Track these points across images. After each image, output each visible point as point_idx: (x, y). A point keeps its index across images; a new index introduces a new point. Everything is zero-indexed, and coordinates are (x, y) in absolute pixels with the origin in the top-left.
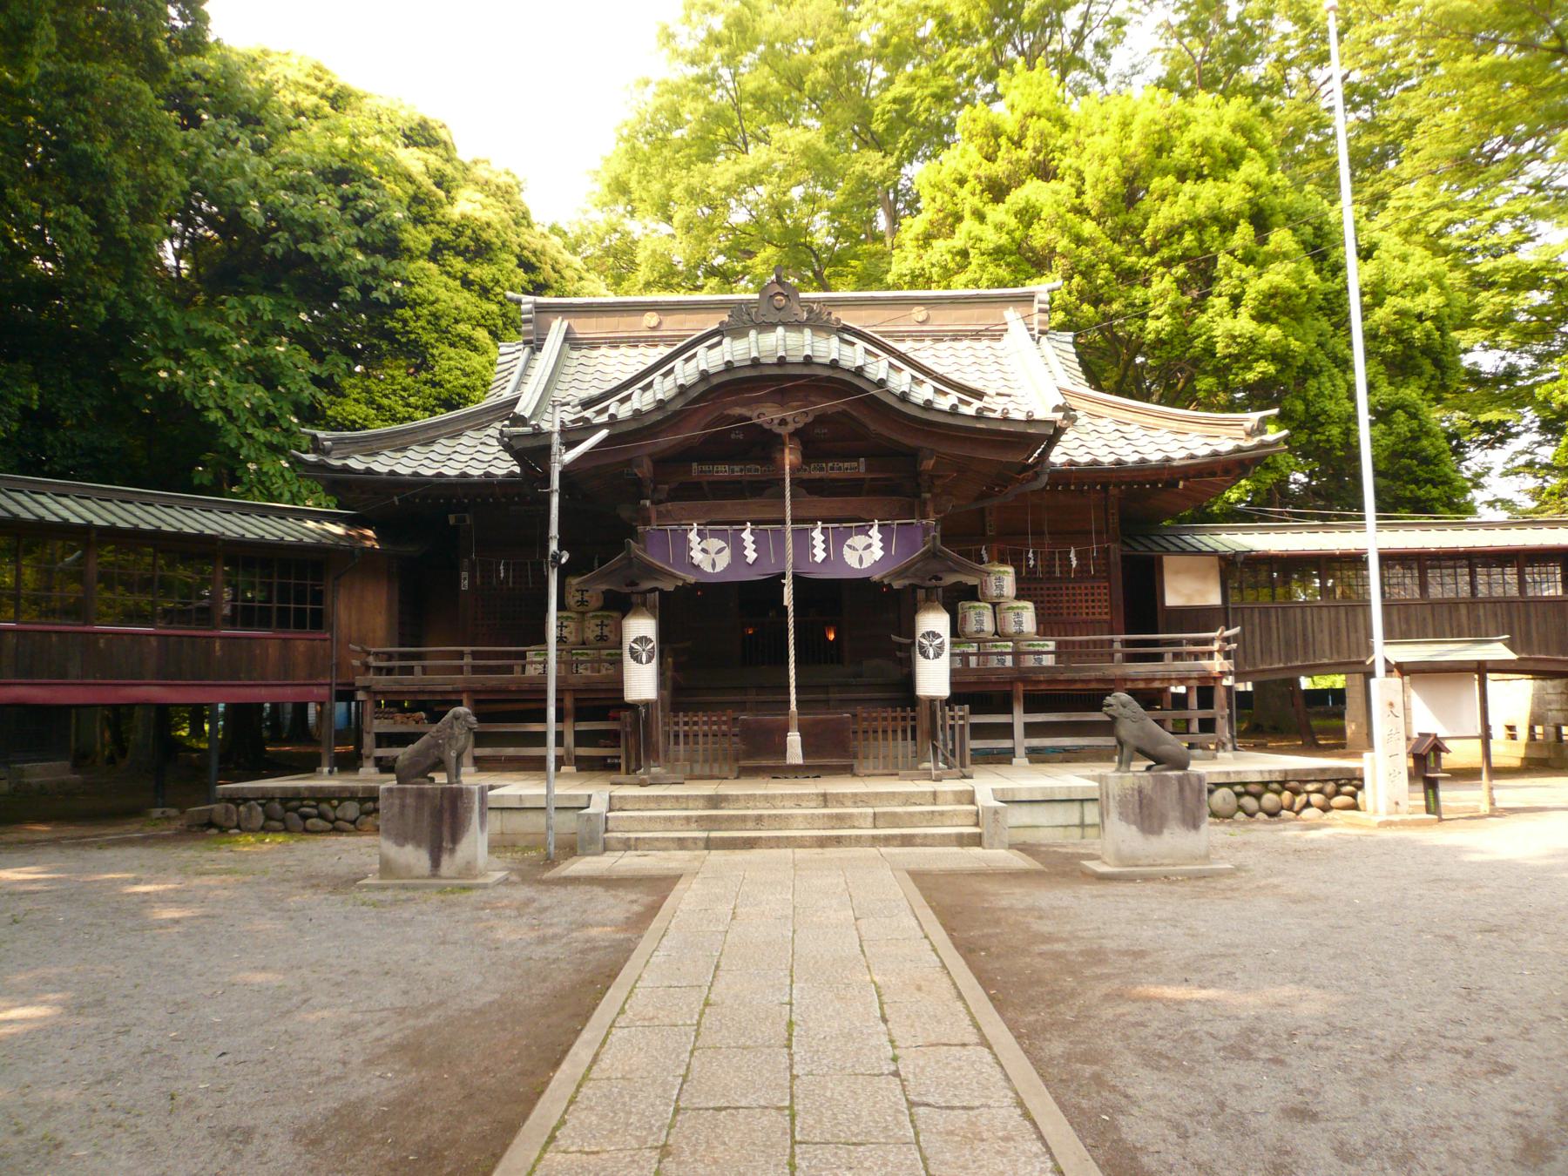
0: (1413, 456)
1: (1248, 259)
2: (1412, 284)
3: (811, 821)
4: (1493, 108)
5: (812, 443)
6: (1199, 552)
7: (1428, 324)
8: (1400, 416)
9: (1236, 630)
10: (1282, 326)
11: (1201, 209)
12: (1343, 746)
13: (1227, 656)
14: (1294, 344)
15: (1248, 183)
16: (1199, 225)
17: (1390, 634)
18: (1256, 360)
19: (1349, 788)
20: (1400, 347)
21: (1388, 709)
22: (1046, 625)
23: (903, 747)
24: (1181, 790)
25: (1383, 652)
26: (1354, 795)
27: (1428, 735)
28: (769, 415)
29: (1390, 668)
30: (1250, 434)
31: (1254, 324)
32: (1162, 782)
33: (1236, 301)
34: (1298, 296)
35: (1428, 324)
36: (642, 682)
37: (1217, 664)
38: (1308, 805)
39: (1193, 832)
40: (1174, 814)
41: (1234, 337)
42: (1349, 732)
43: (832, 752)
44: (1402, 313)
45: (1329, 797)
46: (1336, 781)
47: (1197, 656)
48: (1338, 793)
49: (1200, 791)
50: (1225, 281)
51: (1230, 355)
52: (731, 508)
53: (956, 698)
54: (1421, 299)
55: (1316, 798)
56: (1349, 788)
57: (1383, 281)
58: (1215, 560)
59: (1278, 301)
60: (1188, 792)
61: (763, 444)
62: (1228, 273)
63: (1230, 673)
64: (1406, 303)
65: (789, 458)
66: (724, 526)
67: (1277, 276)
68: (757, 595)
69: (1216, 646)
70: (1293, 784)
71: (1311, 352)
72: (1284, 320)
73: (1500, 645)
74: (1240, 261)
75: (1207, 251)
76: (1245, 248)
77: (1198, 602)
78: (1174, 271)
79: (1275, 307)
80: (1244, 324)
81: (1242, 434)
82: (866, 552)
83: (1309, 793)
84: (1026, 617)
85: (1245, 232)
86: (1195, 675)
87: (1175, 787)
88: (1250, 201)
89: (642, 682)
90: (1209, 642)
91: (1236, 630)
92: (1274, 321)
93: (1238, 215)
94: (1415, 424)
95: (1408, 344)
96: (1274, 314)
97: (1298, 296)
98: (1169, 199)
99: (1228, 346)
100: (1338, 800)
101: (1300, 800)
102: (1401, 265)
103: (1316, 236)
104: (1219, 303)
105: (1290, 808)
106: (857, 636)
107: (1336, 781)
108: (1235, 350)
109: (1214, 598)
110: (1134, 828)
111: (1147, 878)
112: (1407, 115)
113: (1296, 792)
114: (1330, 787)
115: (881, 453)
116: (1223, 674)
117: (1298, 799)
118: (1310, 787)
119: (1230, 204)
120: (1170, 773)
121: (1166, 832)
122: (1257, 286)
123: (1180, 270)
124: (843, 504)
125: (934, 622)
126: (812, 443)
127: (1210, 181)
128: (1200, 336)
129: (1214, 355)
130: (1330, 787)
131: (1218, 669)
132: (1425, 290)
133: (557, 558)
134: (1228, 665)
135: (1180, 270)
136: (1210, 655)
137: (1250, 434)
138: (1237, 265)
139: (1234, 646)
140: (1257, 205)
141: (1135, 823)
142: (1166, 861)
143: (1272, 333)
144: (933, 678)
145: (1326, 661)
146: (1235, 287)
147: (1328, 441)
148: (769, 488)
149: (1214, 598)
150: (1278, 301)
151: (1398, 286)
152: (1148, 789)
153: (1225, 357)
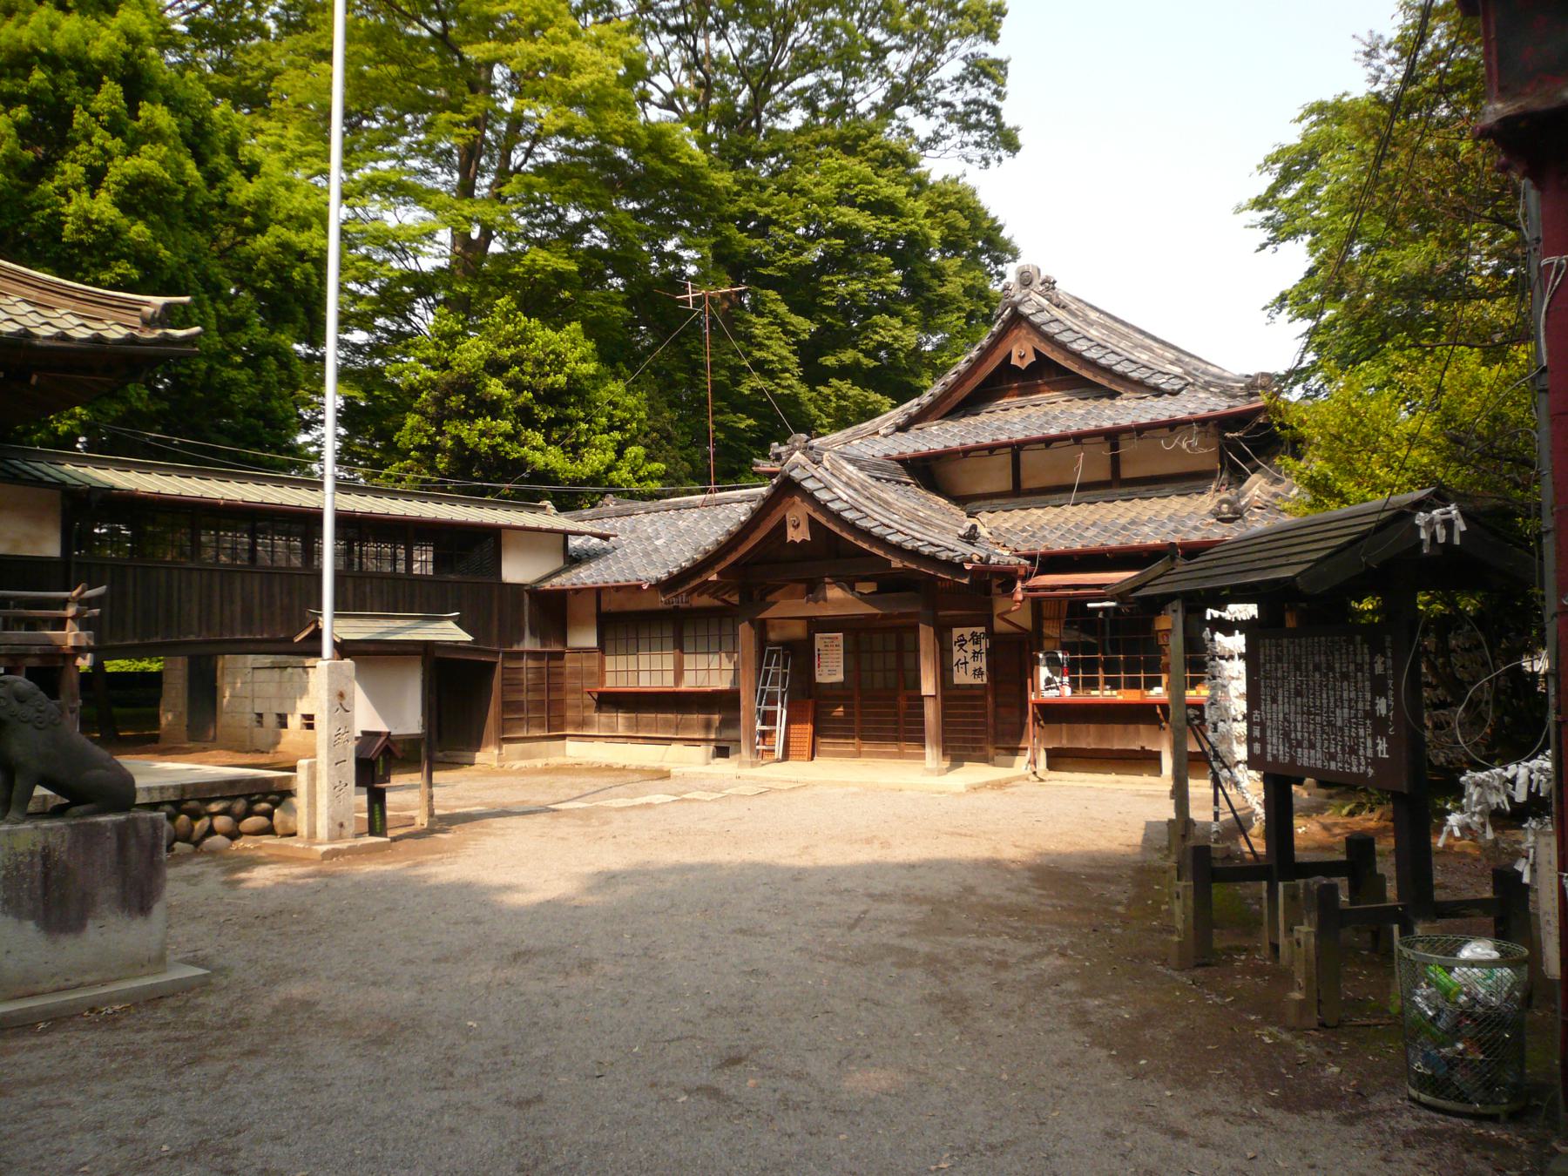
0: (261, 415)
1: (115, 128)
2: (297, 217)
6: (39, 482)
7: (308, 265)
8: (271, 363)
9: (101, 590)
10: (150, 225)
11: (60, 42)
12: (155, 739)
13: (85, 624)
14: (164, 253)
15: (126, 33)
16: (53, 61)
17: (343, 607)
18: (117, 259)
19: (264, 806)
20: (279, 285)
21: (337, 701)
24: (122, 848)
25: (332, 627)
26: (269, 815)
27: (378, 734)
29: (344, 649)
30: (149, 323)
31: (116, 211)
32: (90, 836)
33: (95, 178)
34: (174, 192)
35: (308, 265)
37: (71, 636)
38: (211, 831)
39: (140, 919)
40: (107, 892)
41: (88, 221)
42: (163, 721)
44: (285, 247)
45: (239, 819)
46: (248, 797)
47: (32, 624)
48: (249, 813)
49: (155, 847)
50: (83, 147)
51: (80, 244)
54: (305, 236)
55: (221, 822)
56: (264, 806)
57: (268, 203)
58: (58, 493)
59: (148, 191)
60: (133, 851)
62: (88, 137)
63: (90, 649)
64: (291, 236)
67: (147, 161)
69: (71, 611)
70: (192, 804)
71: (181, 268)
72: (154, 218)
73: (450, 624)
74: (104, 128)
75: (61, 99)
76: (112, 114)
77: (27, 551)
78: (12, 112)
79: (144, 198)
80: (103, 207)
81: (137, 321)
83: (213, 815)
85: (109, 95)
86: (36, 650)
87: (112, 844)
88: (126, 55)
90: (64, 603)
91: (101, 590)
92: (142, 217)
93: (106, 66)
94: (284, 375)
95: (287, 282)
96: (142, 208)
97: (174, 192)
98: (19, 16)
99: (79, 231)
100: (251, 822)
101: (201, 825)
102: (287, 194)
103: (195, 134)
104: (71, 170)
105: (186, 838)
107: (248, 797)
108: (88, 238)
109: (51, 548)
110: (30, 925)
111: (57, 1020)
112: (267, 64)
113: (195, 816)
114: (240, 806)
116: (78, 651)
117: (198, 825)
118: (214, 807)
119: (98, 51)
120: (102, 819)
121: (91, 926)
122: (124, 168)
123: (22, 113)
127: (75, 17)
128: (42, 208)
129: (58, 239)
130: (240, 806)
131: (71, 642)
132: (310, 228)
134: (85, 638)
135: (22, 113)
136: (60, 624)
137: (149, 323)
138: (100, 131)
139: (96, 611)
140: (134, 65)
141: (32, 916)
142: (88, 978)
143: (138, 231)
145: (192, 638)
146: (95, 157)
147: (191, 376)
149: (51, 548)
150: (148, 191)
151: (281, 216)
152: (61, 849)
153: (73, 245)
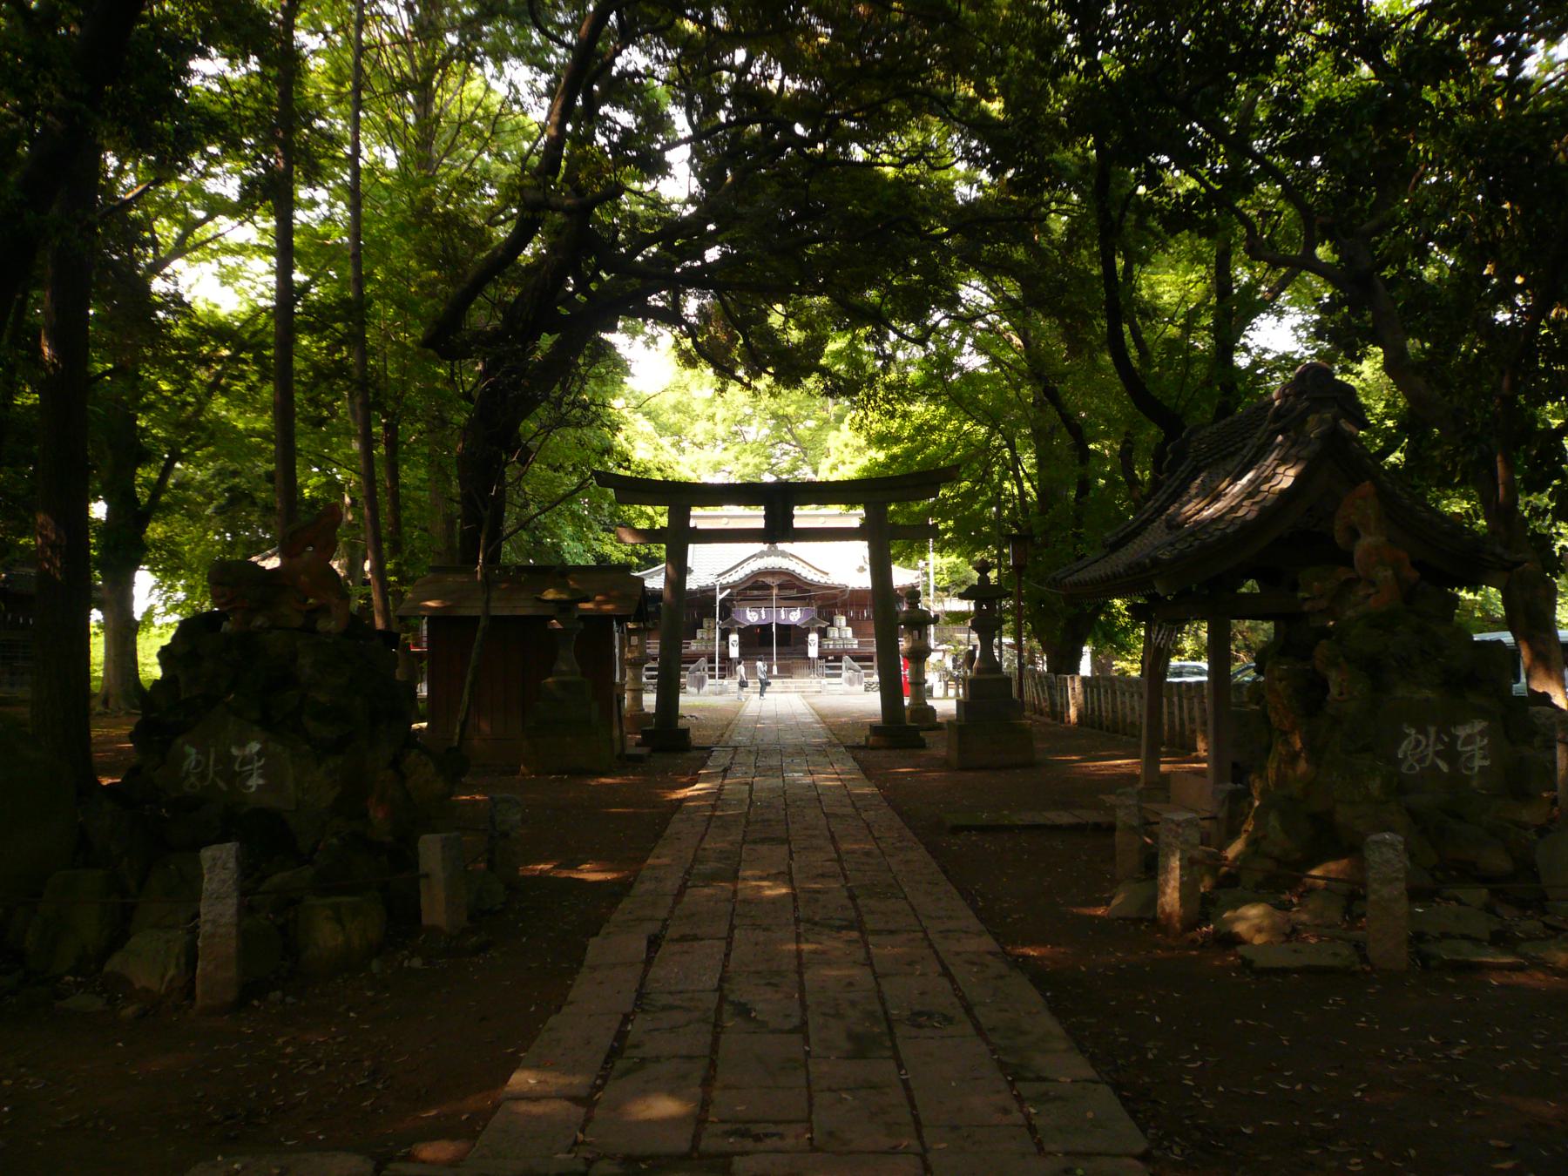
3: (1123, 703)
4: (440, 91)
5: (781, 587)
22: (855, 634)
23: (806, 671)
28: (769, 580)
36: (734, 652)
43: (786, 672)
52: (758, 603)
53: (820, 658)
61: (769, 587)
65: (775, 592)
66: (756, 608)
68: (766, 628)
82: (795, 617)
84: (849, 632)
89: (734, 652)
106: (791, 639)
115: (800, 590)
124: (789, 602)
125: (813, 637)
126: (781, 587)
133: (599, 603)
144: (813, 652)
148: (768, 598)
